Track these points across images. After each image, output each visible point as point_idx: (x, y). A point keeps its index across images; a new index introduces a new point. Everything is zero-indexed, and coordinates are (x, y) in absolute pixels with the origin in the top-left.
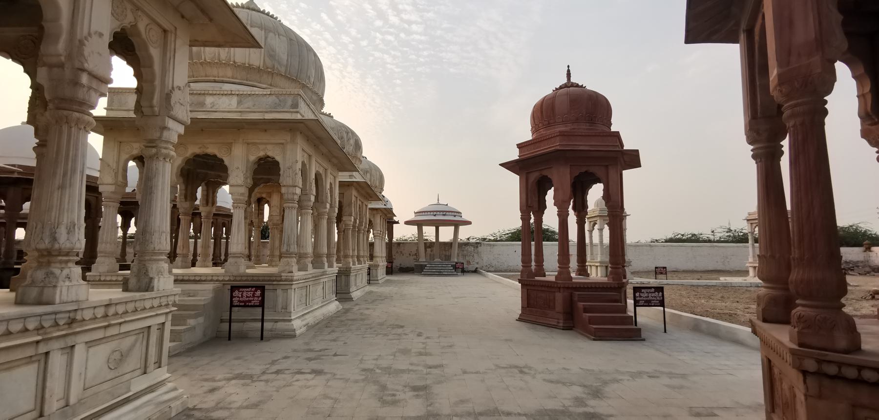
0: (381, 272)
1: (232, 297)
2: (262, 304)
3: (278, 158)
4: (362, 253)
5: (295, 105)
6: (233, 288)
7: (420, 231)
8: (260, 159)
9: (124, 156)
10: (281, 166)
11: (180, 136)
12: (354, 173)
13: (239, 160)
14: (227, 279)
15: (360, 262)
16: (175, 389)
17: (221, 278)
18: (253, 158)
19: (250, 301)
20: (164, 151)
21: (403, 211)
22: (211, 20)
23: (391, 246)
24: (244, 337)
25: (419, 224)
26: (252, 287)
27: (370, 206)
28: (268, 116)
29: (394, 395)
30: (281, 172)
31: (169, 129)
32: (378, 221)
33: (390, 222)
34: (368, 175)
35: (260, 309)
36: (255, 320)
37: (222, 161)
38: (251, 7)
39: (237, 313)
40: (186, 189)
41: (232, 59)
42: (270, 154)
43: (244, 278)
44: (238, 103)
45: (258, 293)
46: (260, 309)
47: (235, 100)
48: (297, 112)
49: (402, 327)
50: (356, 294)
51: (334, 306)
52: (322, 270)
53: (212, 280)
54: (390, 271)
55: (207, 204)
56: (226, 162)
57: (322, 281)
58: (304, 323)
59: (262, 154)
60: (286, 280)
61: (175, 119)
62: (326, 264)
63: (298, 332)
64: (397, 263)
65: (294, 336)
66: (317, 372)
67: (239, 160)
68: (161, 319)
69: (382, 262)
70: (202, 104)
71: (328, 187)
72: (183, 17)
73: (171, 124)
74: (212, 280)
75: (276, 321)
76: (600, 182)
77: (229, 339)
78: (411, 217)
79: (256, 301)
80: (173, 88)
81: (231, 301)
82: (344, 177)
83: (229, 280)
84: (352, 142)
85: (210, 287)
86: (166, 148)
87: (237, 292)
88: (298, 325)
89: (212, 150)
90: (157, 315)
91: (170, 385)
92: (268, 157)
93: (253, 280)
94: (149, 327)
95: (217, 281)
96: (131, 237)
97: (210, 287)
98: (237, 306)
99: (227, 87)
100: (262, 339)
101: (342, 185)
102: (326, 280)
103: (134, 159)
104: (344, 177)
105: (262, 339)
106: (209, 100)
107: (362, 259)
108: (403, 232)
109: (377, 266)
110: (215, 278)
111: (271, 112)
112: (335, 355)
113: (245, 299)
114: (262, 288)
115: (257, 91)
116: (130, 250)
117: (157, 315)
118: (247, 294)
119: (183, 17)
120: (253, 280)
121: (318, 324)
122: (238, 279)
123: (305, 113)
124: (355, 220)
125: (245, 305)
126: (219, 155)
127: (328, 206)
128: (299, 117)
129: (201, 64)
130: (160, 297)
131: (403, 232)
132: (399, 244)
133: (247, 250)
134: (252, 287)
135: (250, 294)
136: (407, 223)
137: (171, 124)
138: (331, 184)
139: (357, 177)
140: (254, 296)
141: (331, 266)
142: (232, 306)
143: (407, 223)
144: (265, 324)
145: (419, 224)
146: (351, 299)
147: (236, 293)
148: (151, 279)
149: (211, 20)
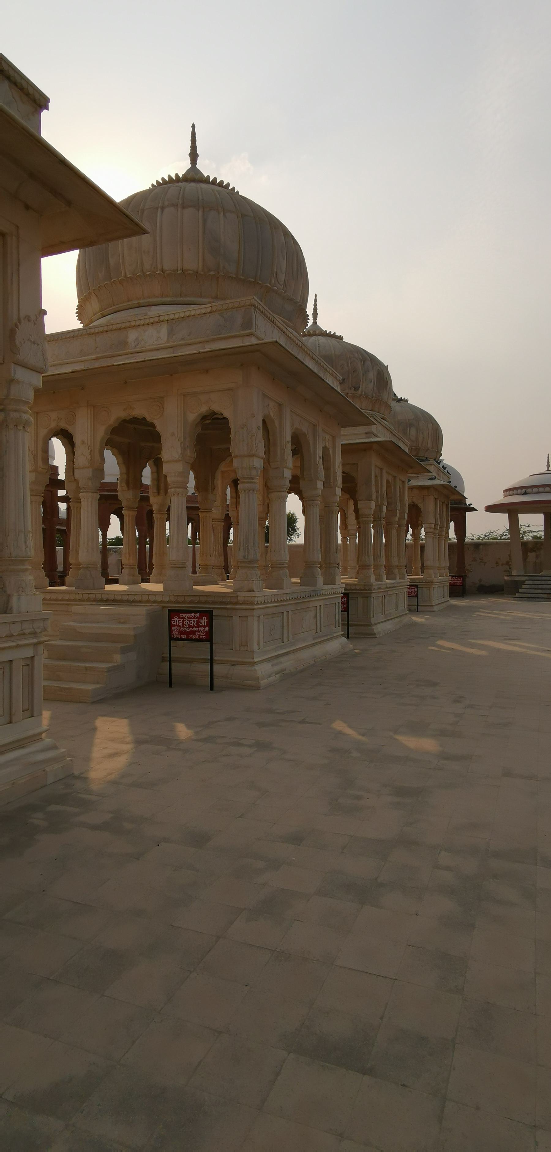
0: (438, 593)
1: (171, 626)
2: (209, 638)
3: (227, 414)
4: (395, 561)
5: (248, 324)
6: (173, 613)
7: (514, 522)
8: (204, 418)
9: (43, 432)
10: (232, 425)
11: (37, 391)
12: (373, 429)
13: (174, 426)
14: (167, 599)
15: (390, 574)
16: (54, 747)
17: (159, 599)
18: (192, 417)
19: (193, 633)
20: (13, 415)
21: (482, 488)
22: (69, 203)
23: (462, 551)
24: (188, 684)
25: (512, 511)
26: (196, 612)
27: (414, 483)
28: (209, 347)
29: (359, 798)
30: (232, 436)
31: (18, 382)
32: (430, 507)
33: (458, 509)
34: (413, 431)
35: (208, 644)
36: (204, 660)
37: (153, 426)
38: (197, 177)
39: (180, 649)
40: (128, 473)
41: (159, 267)
42: (215, 408)
43: (188, 599)
44: (169, 334)
45: (204, 621)
46: (208, 644)
47: (164, 330)
48: (251, 335)
49: (435, 684)
50: (382, 628)
51: (337, 644)
52: (313, 588)
53: (148, 601)
54: (458, 590)
55: (159, 493)
56: (159, 428)
57: (312, 604)
58: (277, 668)
59: (204, 409)
60: (244, 603)
61: (25, 366)
62: (320, 579)
63: (263, 682)
64: (474, 578)
65: (257, 688)
66: (261, 746)
67: (174, 426)
68: (29, 652)
69: (441, 578)
70: (124, 343)
71: (320, 453)
72: (27, 207)
73: (20, 374)
74: (148, 601)
75: (233, 664)
76: (50, 336)
77: (170, 686)
78: (499, 498)
79: (202, 633)
80: (19, 320)
81: (170, 632)
82: (354, 435)
83: (170, 602)
84: (372, 375)
85: (141, 611)
86: (16, 411)
87: (176, 618)
88: (264, 671)
89: (139, 411)
90: (18, 646)
91: (48, 741)
92: (214, 413)
93: (199, 602)
94: (11, 661)
95: (155, 602)
96: (111, 544)
97: (141, 611)
98: (177, 639)
99: (154, 311)
100: (212, 688)
101: (348, 450)
102: (321, 603)
103: (56, 435)
104: (354, 435)
105: (212, 688)
106: (132, 336)
107: (396, 571)
108: (481, 525)
109: (429, 583)
110: (152, 598)
111: (214, 340)
112: (302, 722)
113: (187, 629)
114: (209, 614)
115: (193, 310)
116: (112, 559)
117: (18, 646)
118: (189, 622)
119: (27, 207)
120: (199, 602)
121: (302, 671)
122: (181, 599)
123: (266, 332)
124: (379, 507)
125: (189, 637)
126: (149, 419)
127: (320, 485)
128: (254, 341)
129: (121, 282)
130: (22, 622)
131: (481, 525)
132: (477, 546)
133: (222, 559)
134: (196, 612)
135: (194, 622)
136: (490, 509)
137: (20, 374)
138: (325, 449)
139: (381, 435)
140: (198, 626)
141: (330, 580)
142: (171, 639)
143: (490, 509)
144: (216, 667)
145: (512, 511)
146: (372, 635)
147: (176, 621)
148: (9, 596)
149: (69, 203)
